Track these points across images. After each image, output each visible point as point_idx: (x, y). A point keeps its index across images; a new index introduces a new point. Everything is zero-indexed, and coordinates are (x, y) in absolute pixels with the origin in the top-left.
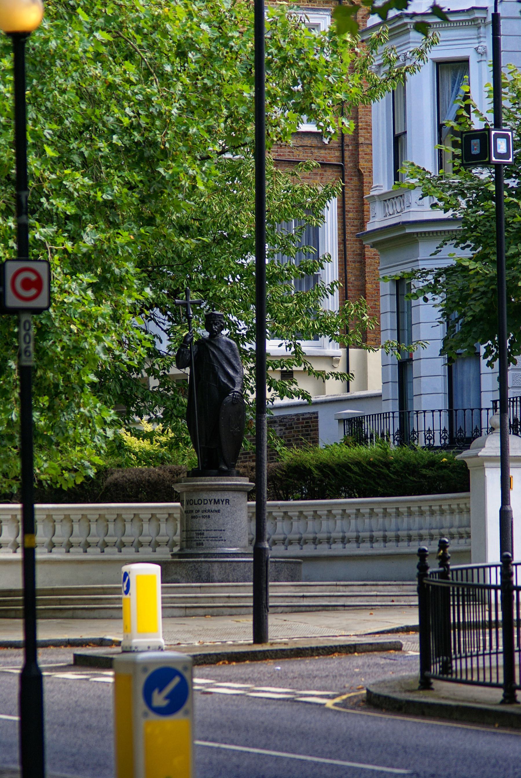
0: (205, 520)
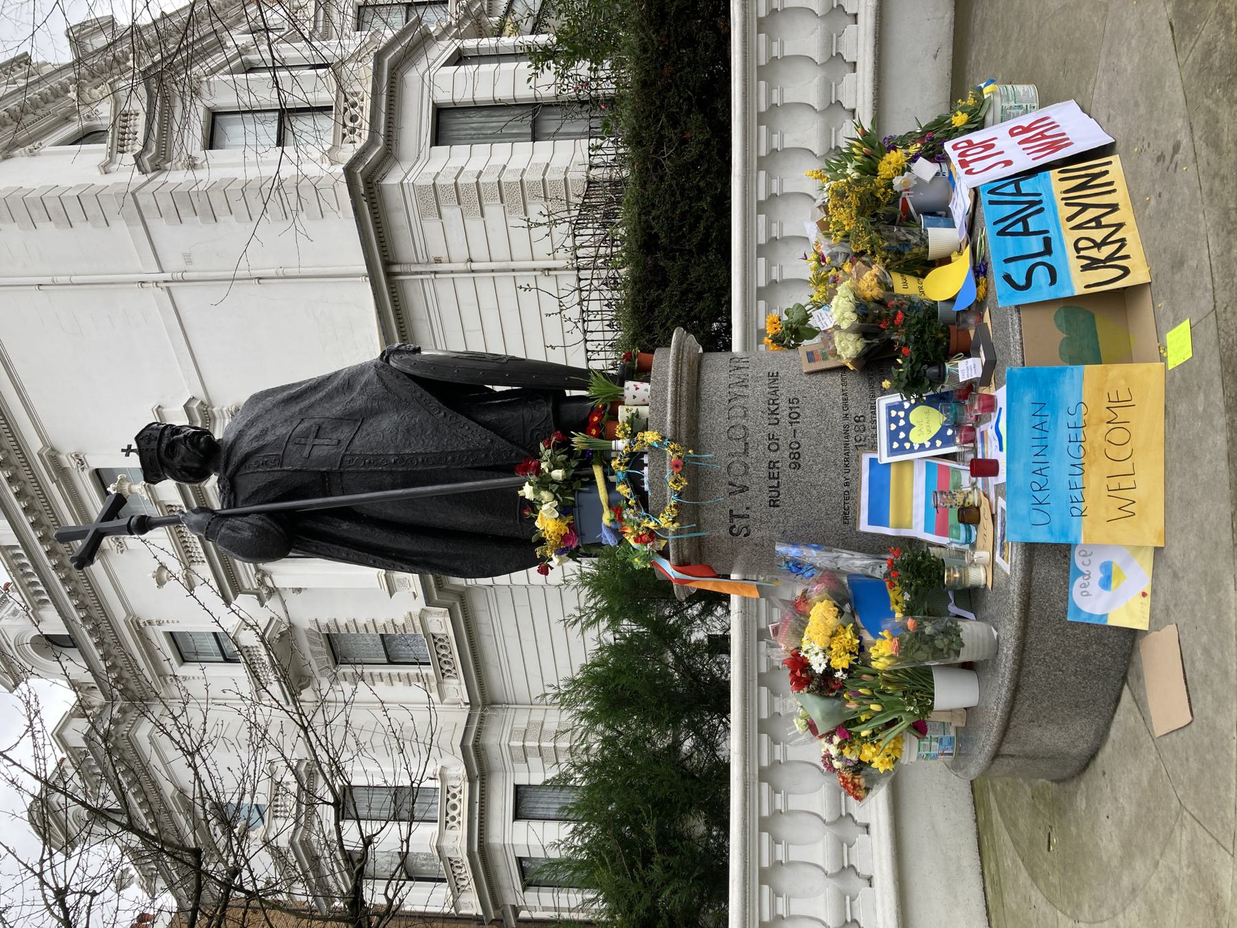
0: (807, 412)
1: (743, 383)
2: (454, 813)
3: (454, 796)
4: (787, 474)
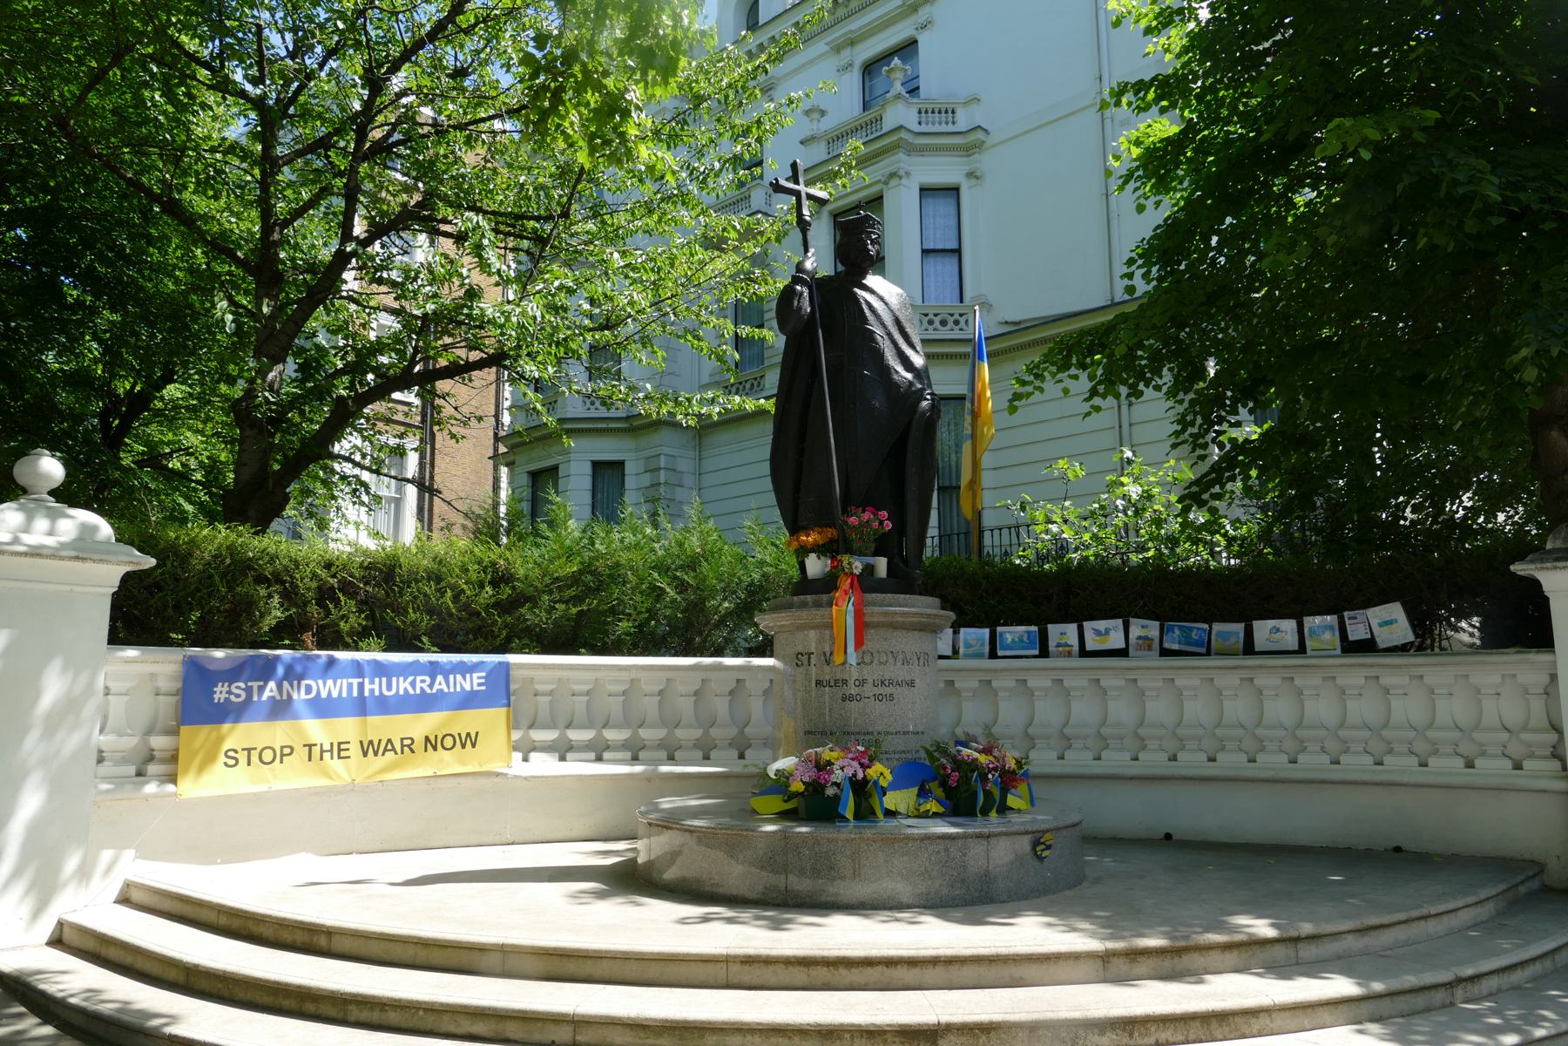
1: (905, 662)
2: (937, 324)
3: (956, 323)
4: (839, 692)
